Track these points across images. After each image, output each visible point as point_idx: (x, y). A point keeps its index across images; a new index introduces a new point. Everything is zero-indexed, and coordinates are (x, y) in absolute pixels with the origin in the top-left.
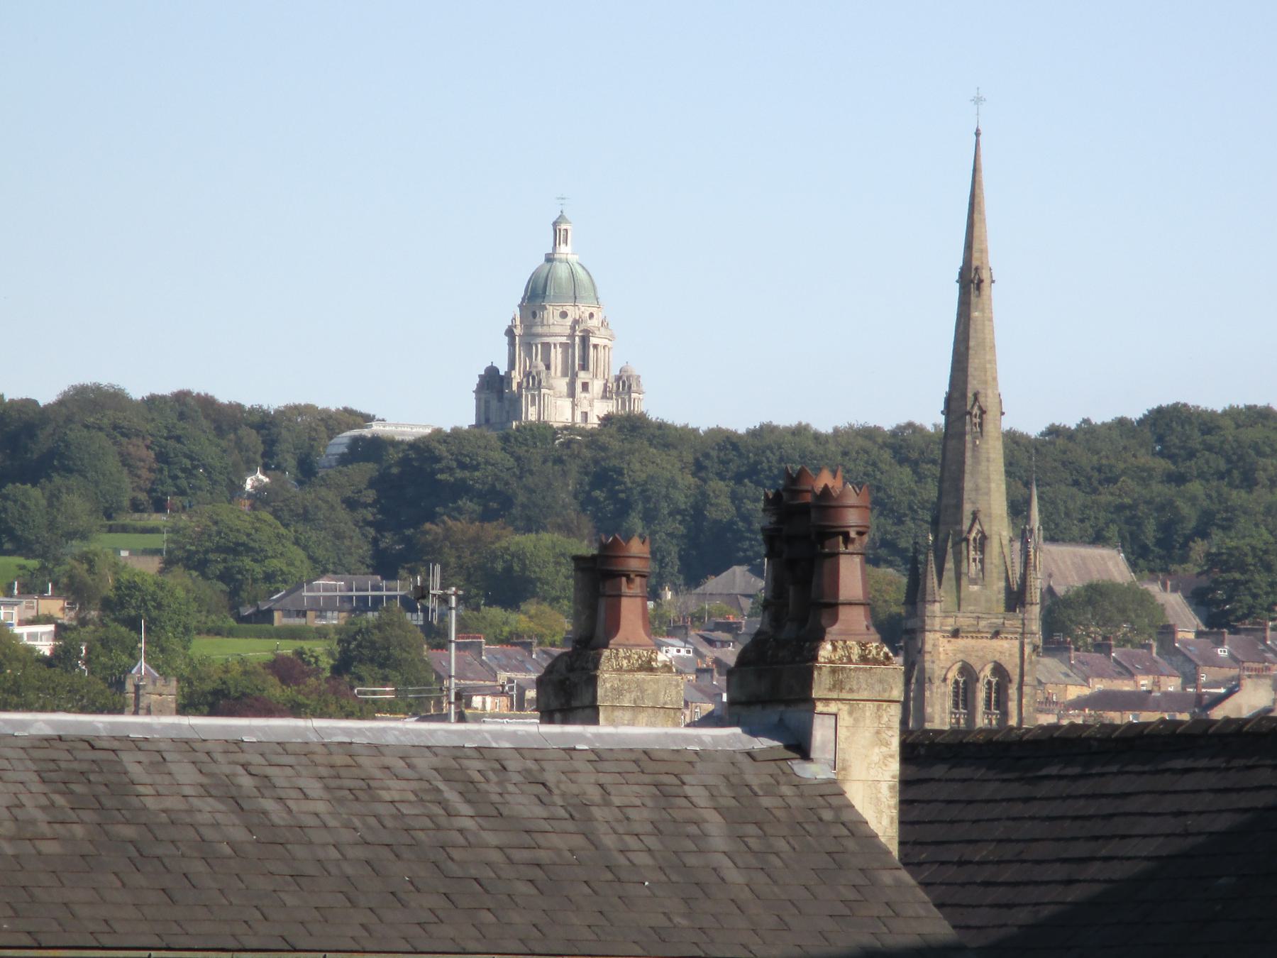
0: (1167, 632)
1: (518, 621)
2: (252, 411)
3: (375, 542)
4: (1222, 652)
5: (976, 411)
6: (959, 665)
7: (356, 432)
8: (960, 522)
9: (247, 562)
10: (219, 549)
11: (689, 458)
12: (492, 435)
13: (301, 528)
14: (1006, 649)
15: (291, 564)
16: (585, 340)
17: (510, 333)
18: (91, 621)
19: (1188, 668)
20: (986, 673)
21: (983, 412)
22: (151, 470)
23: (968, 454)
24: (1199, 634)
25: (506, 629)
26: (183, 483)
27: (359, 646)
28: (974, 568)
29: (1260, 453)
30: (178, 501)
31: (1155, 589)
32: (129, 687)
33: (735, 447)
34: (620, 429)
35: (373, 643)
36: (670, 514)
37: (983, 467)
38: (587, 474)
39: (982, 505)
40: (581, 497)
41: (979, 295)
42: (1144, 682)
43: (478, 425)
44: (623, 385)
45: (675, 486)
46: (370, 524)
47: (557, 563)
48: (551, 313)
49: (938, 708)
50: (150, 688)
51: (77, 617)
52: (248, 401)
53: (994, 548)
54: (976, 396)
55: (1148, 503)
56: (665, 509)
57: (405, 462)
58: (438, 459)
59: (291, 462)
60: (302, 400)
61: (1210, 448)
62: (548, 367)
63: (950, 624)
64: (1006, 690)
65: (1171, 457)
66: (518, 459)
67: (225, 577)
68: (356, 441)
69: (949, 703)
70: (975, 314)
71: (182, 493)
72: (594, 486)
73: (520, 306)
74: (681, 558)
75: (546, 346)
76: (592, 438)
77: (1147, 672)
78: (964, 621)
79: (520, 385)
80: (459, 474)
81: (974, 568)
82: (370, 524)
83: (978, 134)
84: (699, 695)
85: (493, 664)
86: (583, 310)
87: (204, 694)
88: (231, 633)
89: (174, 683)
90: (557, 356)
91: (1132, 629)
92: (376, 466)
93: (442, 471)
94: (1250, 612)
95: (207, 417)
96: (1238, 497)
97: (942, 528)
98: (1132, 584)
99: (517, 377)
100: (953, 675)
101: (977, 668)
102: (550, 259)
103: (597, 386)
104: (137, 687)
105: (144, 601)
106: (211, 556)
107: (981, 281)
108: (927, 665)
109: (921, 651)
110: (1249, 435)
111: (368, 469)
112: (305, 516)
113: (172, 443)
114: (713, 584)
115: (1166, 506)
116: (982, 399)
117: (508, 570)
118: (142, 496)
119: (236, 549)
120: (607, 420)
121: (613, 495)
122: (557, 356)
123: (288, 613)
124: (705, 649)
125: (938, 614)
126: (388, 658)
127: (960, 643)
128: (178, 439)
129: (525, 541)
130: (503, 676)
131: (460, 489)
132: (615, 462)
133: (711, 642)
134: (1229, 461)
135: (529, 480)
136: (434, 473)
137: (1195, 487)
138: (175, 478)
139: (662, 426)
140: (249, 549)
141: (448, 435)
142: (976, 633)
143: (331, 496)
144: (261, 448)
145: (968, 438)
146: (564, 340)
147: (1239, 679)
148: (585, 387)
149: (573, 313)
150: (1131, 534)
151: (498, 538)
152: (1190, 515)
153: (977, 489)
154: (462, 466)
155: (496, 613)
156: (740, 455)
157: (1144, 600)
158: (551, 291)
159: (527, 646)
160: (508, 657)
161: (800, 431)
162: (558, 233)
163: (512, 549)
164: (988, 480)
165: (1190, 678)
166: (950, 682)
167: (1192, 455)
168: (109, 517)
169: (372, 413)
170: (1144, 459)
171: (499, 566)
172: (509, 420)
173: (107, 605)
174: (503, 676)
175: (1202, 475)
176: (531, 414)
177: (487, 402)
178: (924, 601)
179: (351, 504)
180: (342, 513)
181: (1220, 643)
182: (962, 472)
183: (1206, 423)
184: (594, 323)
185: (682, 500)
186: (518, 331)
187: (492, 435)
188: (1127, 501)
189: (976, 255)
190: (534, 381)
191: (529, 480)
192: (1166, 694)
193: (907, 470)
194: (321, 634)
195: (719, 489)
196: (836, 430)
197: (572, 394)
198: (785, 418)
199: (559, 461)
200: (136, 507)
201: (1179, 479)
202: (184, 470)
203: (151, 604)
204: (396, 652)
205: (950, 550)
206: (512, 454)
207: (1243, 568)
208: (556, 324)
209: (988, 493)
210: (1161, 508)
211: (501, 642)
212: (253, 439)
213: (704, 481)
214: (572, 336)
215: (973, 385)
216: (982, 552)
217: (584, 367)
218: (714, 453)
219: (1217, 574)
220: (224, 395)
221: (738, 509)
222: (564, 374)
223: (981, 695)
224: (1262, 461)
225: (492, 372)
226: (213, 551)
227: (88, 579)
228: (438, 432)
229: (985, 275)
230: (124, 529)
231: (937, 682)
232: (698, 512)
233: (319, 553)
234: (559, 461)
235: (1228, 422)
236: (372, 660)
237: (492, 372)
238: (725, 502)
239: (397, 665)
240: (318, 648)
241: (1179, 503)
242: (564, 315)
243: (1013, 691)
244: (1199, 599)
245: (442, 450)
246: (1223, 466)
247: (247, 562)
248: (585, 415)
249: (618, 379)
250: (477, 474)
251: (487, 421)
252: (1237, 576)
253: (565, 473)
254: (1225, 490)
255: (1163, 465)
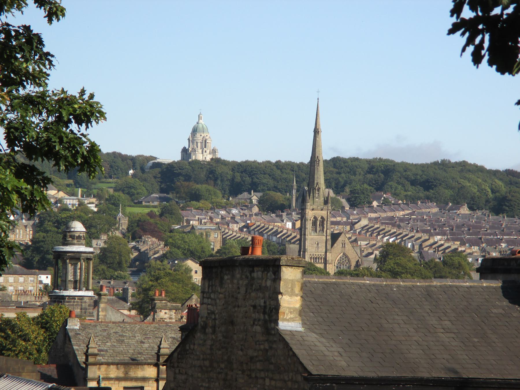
0: (343, 208)
1: (200, 204)
2: (130, 156)
3: (160, 186)
4: (355, 212)
5: (318, 160)
6: (320, 217)
7: (154, 161)
8: (314, 185)
9: (133, 190)
10: (127, 187)
11: (230, 167)
12: (186, 162)
13: (144, 182)
14: (324, 213)
15: (143, 190)
16: (205, 141)
17: (189, 139)
18: (102, 204)
19: (348, 216)
20: (319, 218)
21: (319, 161)
22: (108, 169)
23: (316, 170)
24: (349, 208)
25: (197, 206)
26: (115, 172)
27: (165, 210)
28: (317, 195)
29: (357, 167)
30: (115, 176)
31: (339, 198)
32: (118, 219)
33: (241, 165)
34: (215, 161)
35: (169, 209)
36: (227, 180)
37: (319, 173)
38: (208, 171)
39: (319, 181)
40: (207, 176)
41: (318, 135)
42: (339, 219)
43: (182, 160)
44: (214, 151)
45: (228, 174)
46: (159, 182)
47: (206, 191)
48: (198, 135)
49: (309, 226)
50: (122, 219)
51: (99, 203)
52: (129, 154)
53: (321, 190)
54: (318, 157)
55: (333, 178)
56: (225, 179)
57: (167, 168)
58: (175, 168)
59: (139, 168)
60: (141, 154)
61: (346, 167)
62: (197, 147)
63: (312, 208)
64: (324, 222)
65: (337, 168)
66: (192, 168)
67: (128, 193)
68: (154, 163)
69: (311, 225)
70: (317, 139)
71: (115, 174)
72: (210, 174)
73: (191, 134)
74: (229, 190)
75: (197, 143)
76: (208, 163)
77: (339, 216)
78: (315, 207)
79: (191, 151)
80: (179, 171)
81: (317, 195)
82: (159, 182)
83: (318, 99)
84: (241, 221)
85: (195, 214)
86: (205, 134)
87: (135, 221)
88: (133, 206)
89: (127, 218)
90: (199, 144)
91: (335, 207)
92: (160, 169)
93: (175, 170)
94: (360, 203)
95: (120, 157)
96: (353, 177)
97: (310, 186)
98: (335, 197)
99: (190, 149)
100: (312, 219)
101: (318, 217)
102: (198, 123)
103: (208, 152)
104: (119, 219)
105: (115, 199)
106: (125, 189)
107: (319, 132)
108: (307, 217)
109: (305, 214)
110: (354, 163)
111: (158, 170)
112: (145, 180)
113: (113, 163)
114: (240, 196)
115: (337, 179)
116: (319, 158)
117: (196, 193)
118: (107, 175)
119: (130, 188)
120: (212, 159)
121: (214, 176)
122: (199, 144)
123: (146, 202)
124: (241, 211)
125: (309, 205)
126: (172, 213)
127: (314, 212)
128: (115, 162)
129: (199, 186)
130: (197, 217)
131: (180, 174)
132: (214, 169)
133: (242, 209)
134: (350, 169)
135: (195, 172)
136: (174, 170)
137: (343, 175)
138: (114, 171)
139: (224, 161)
140: (133, 187)
141: (177, 162)
142: (317, 209)
143: (151, 176)
144: (132, 164)
145: (316, 166)
146: (201, 141)
147: (361, 218)
148: (206, 152)
149: (203, 135)
150: (329, 185)
151: (193, 186)
152: (342, 182)
153: (318, 178)
154: (180, 169)
155: (194, 203)
156: (242, 167)
157: (338, 201)
158: (198, 130)
159: (202, 210)
160: (198, 212)
161: (255, 162)
162: (199, 118)
163: (197, 188)
164: (320, 176)
165: (348, 218)
166: (311, 220)
167: (342, 168)
168: (99, 180)
169: (156, 157)
170: (332, 169)
171: (193, 192)
172: (189, 159)
173: (107, 200)
174: (197, 217)
175: (344, 172)
176: (193, 158)
177: (184, 155)
178: (306, 202)
179: (155, 177)
180: (153, 179)
181: (355, 210)
182: (314, 174)
183: (344, 161)
184: (207, 137)
185: (229, 178)
186: (191, 139)
187: (186, 162)
188: (328, 178)
189: (318, 126)
190: (194, 150)
191: (195, 172)
192: (344, 222)
193: (279, 171)
194: (155, 207)
195: (238, 175)
196: (263, 162)
197: (203, 153)
198: (251, 159)
199: (202, 168)
200: (105, 177)
201: (339, 173)
202: (116, 169)
203: (117, 200)
204: (174, 211)
205: (312, 191)
206: (191, 166)
207: (358, 194)
208: (199, 137)
209: (320, 179)
210: (336, 180)
211: (196, 209)
212: (130, 162)
213: (234, 173)
214: (203, 140)
215: (317, 155)
216: (319, 192)
217: (205, 147)
218: (236, 167)
219: (352, 195)
220: (123, 153)
221: (242, 179)
222: (201, 149)
223: (318, 223)
224: (357, 170)
225: (185, 148)
226: (125, 188)
227: (101, 194)
228: (174, 161)
229: (320, 130)
230: (103, 182)
231: (309, 220)
232: (233, 180)
233: (148, 188)
234: (202, 168)
235: (349, 161)
236: (168, 213)
237: (185, 148)
238: (239, 178)
239: (174, 214)
240: (155, 210)
241: (340, 179)
242: (201, 135)
243: (325, 222)
244: (348, 200)
245: (175, 165)
246: (349, 171)
247: (133, 190)
248: (205, 158)
249: (213, 150)
250: (183, 171)
251: (184, 159)
252: (357, 195)
253: (203, 171)
254: (350, 176)
255: (335, 170)
